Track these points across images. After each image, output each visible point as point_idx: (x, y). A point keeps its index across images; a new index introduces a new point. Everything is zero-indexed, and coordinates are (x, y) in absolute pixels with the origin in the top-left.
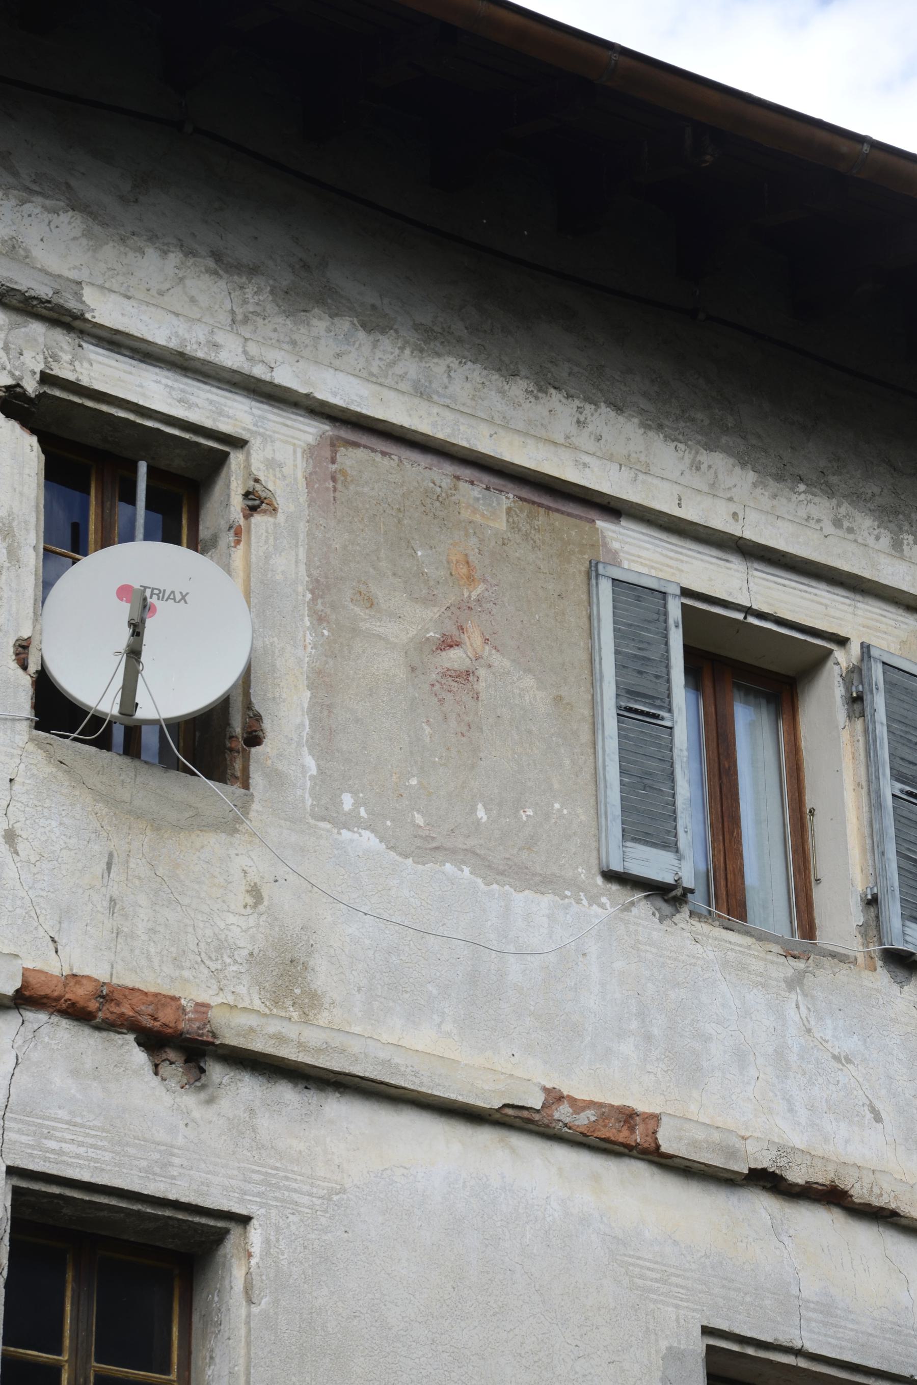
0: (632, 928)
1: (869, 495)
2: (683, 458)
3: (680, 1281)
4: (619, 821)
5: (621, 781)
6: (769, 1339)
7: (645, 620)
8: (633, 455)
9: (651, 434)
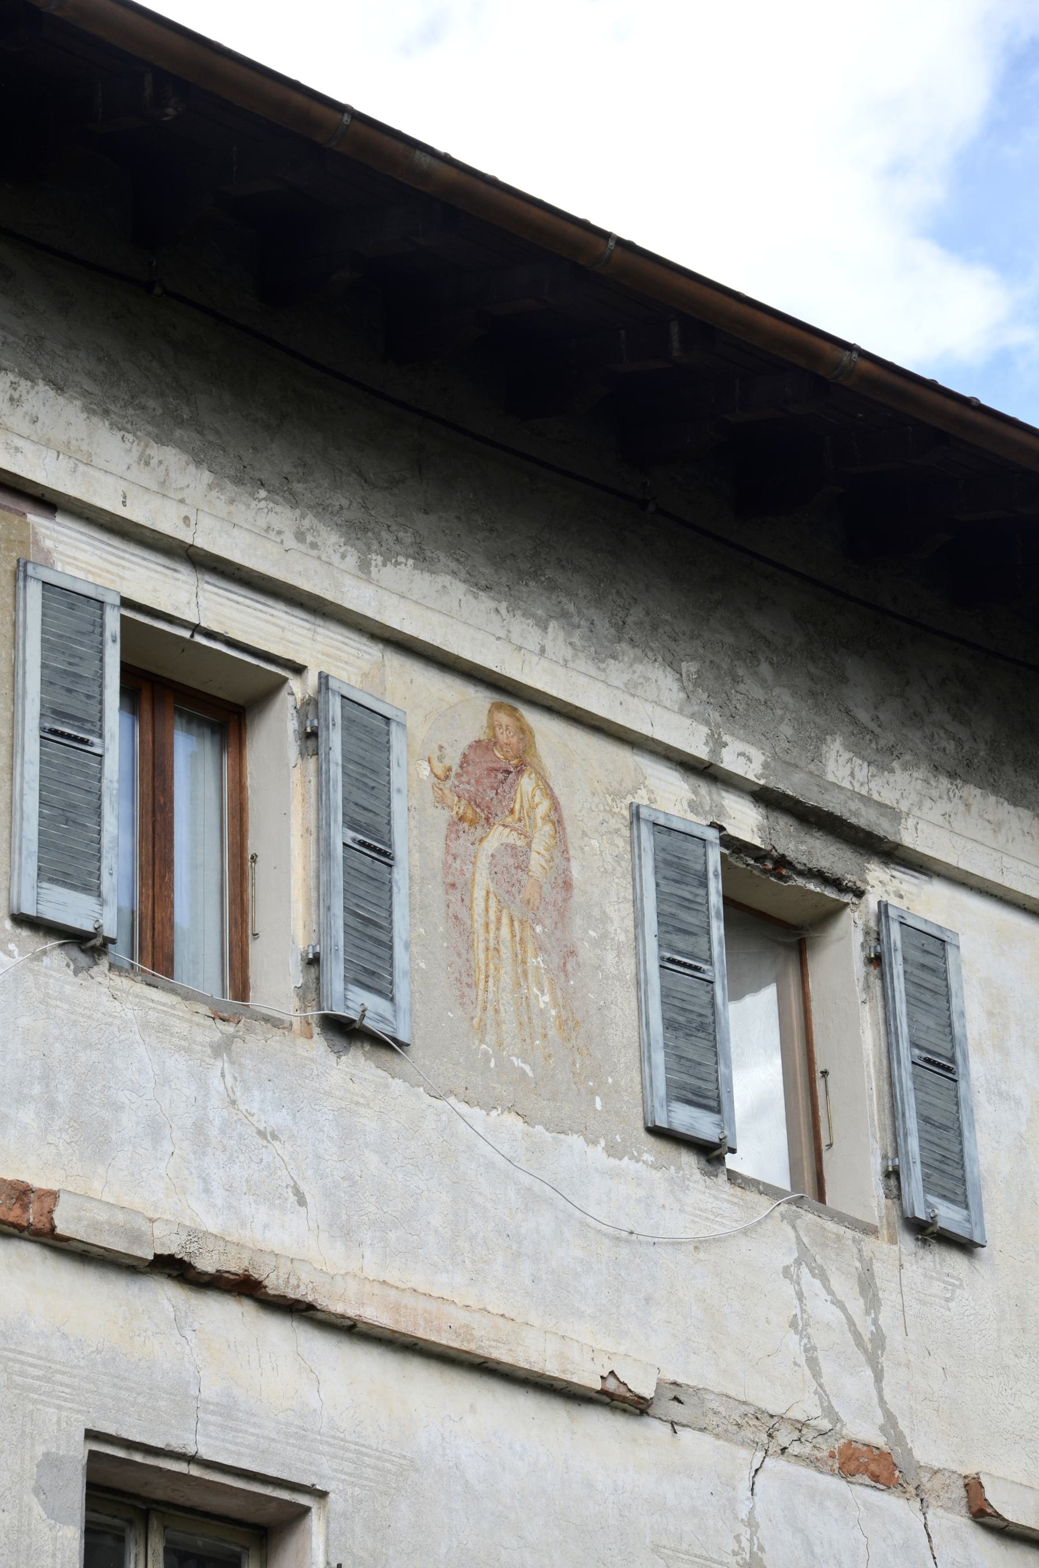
0: (42, 980)
1: (337, 508)
2: (130, 450)
3: (65, 1379)
4: (35, 859)
5: (40, 812)
6: (160, 1445)
7: (78, 632)
8: (74, 442)
9: (95, 420)
